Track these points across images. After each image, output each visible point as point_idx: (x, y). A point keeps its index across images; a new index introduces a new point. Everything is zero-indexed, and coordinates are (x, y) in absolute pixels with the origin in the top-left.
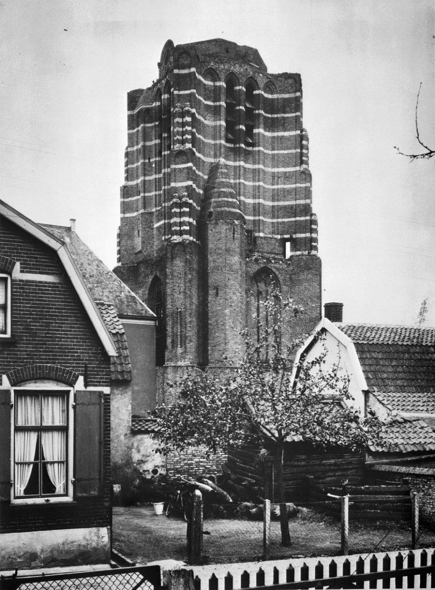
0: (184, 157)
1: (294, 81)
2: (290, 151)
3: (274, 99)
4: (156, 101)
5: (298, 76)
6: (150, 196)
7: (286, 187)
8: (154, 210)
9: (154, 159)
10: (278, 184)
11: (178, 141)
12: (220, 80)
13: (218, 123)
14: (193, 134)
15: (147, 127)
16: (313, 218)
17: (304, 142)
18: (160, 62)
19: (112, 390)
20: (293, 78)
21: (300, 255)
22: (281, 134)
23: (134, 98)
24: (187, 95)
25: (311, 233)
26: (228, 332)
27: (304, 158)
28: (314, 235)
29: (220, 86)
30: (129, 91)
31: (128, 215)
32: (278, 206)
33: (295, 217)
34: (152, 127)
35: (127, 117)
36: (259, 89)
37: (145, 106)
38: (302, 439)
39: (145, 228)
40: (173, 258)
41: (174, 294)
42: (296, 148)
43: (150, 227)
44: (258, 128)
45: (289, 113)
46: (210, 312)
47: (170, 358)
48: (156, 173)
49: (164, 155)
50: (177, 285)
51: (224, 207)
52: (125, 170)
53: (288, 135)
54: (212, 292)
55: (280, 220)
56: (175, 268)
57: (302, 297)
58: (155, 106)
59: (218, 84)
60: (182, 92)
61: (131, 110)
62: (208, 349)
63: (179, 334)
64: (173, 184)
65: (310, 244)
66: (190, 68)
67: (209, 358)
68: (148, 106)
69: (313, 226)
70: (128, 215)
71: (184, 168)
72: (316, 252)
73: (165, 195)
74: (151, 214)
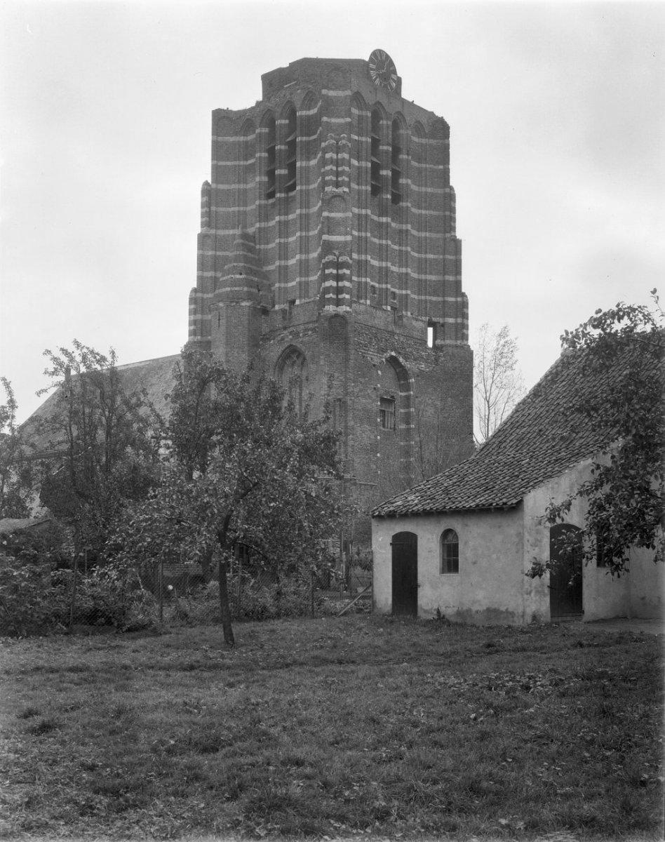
70: (221, 163)
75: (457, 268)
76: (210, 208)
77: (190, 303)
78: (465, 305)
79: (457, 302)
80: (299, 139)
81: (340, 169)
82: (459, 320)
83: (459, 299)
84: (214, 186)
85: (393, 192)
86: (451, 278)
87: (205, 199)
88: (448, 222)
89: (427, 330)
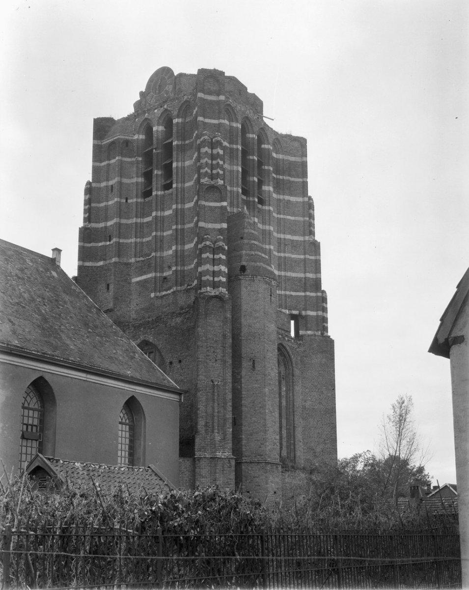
0: (217, 194)
1: (300, 144)
2: (297, 218)
3: (279, 159)
4: (138, 133)
5: (305, 140)
6: (127, 243)
7: (293, 256)
8: (133, 260)
9: (135, 200)
10: (285, 252)
12: (237, 121)
13: (235, 168)
15: (125, 161)
18: (144, 90)
20: (298, 141)
21: (312, 335)
22: (287, 198)
23: (102, 127)
24: (215, 125)
26: (267, 417)
30: (96, 118)
31: (87, 264)
32: (285, 276)
33: (305, 291)
34: (132, 163)
36: (269, 144)
37: (122, 137)
39: (118, 281)
40: (206, 315)
41: (208, 361)
42: (304, 216)
43: (126, 280)
44: (269, 185)
45: (295, 177)
46: (243, 389)
47: (203, 447)
48: (137, 217)
49: (156, 195)
50: (213, 350)
51: (260, 262)
53: (295, 200)
54: (246, 364)
55: (288, 293)
56: (209, 328)
57: (316, 384)
58: (137, 139)
59: (234, 125)
60: (207, 121)
61: (98, 139)
62: (241, 438)
63: (216, 414)
65: (322, 324)
66: (218, 95)
67: (244, 450)
68: (127, 137)
70: (87, 264)
71: (216, 207)
74: (128, 265)
75: (316, 267)
76: (90, 204)
77: (86, 194)
78: (324, 300)
79: (317, 316)
80: (175, 143)
81: (214, 172)
82: (320, 313)
83: (319, 294)
84: (94, 185)
86: (310, 275)
87: (88, 196)
88: (309, 228)
89: (290, 322)
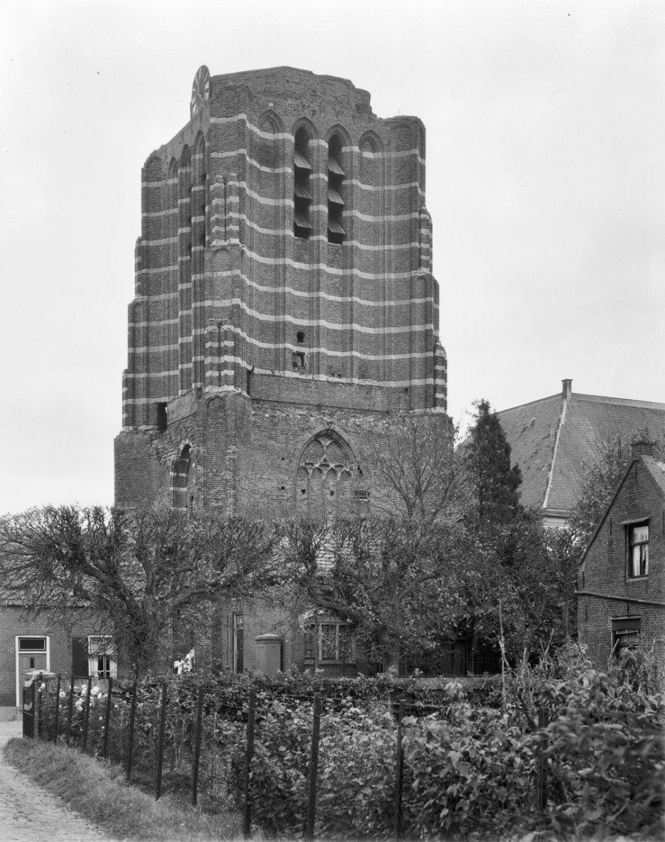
11: (218, 222)
14: (241, 192)
16: (438, 353)
17: (424, 231)
19: (92, 656)
25: (420, 243)
27: (423, 257)
28: (439, 382)
29: (284, 141)
35: (140, 190)
38: (438, 836)
52: (123, 394)
64: (208, 303)
69: (439, 368)
72: (444, 367)
73: (195, 317)
78: (444, 362)
85: (295, 225)
